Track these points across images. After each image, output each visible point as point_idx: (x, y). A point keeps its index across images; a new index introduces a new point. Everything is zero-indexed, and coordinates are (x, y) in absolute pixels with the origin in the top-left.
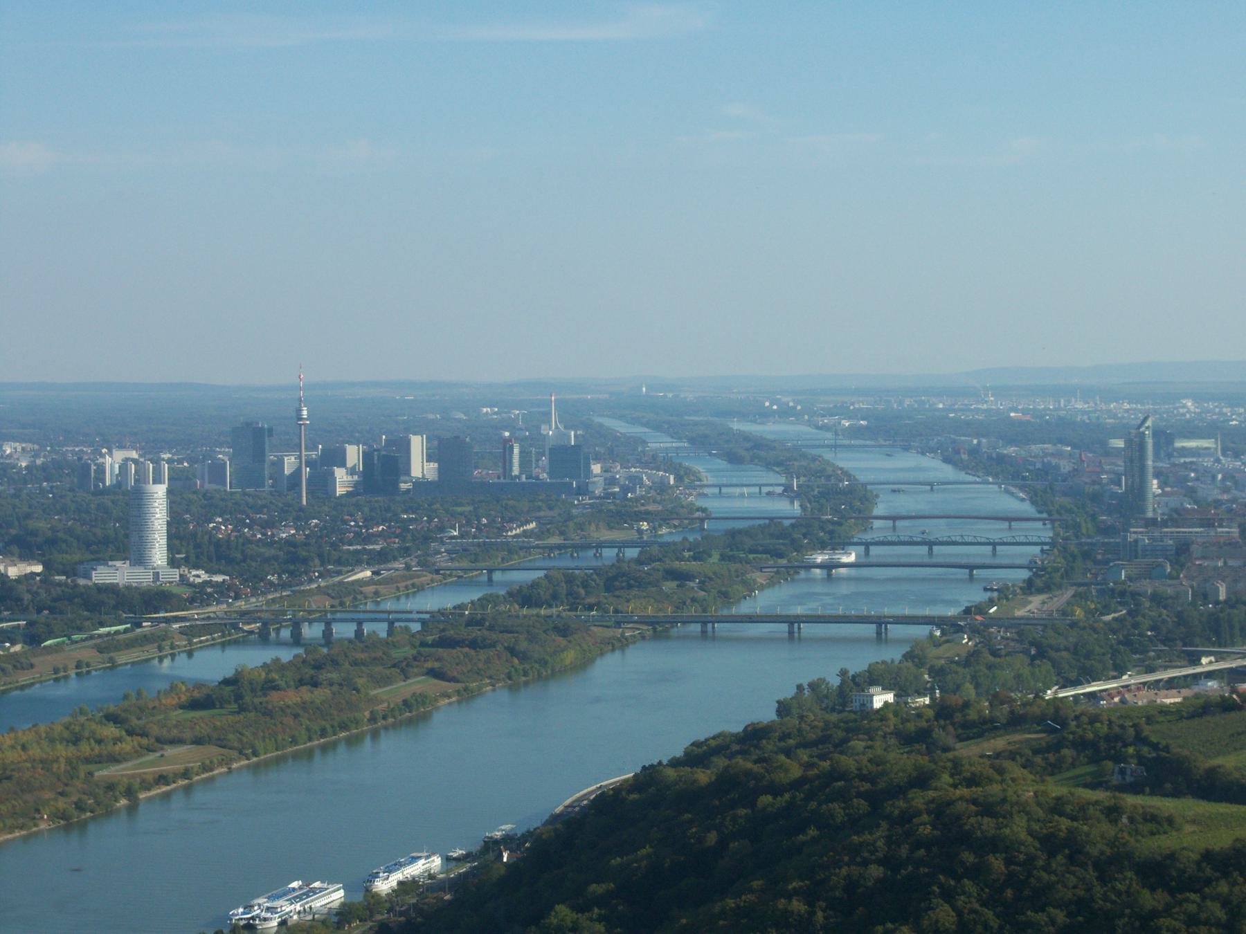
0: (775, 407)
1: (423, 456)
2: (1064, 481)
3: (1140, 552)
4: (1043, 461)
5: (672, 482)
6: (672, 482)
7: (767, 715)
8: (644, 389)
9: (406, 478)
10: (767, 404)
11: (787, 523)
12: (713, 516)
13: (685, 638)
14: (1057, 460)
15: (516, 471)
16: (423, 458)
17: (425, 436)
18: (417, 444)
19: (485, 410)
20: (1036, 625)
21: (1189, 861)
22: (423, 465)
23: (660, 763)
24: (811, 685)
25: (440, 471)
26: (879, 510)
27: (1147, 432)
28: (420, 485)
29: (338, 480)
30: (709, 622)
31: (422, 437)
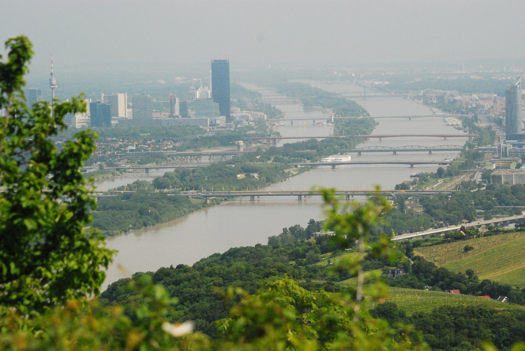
0: (340, 75)
1: (125, 105)
2: (486, 114)
3: (508, 154)
4: (476, 103)
5: (266, 118)
6: (266, 118)
7: (265, 242)
8: (270, 66)
9: (116, 118)
10: (335, 73)
11: (319, 140)
12: (282, 137)
13: (241, 204)
14: (483, 102)
15: (177, 112)
16: (125, 107)
17: (126, 94)
18: (122, 99)
19: (178, 78)
20: (430, 195)
21: (207, 308)
22: (125, 110)
23: (171, 267)
24: (290, 229)
25: (134, 113)
26: (375, 132)
27: (518, 86)
28: (123, 121)
29: (77, 119)
30: (302, 195)
31: (125, 94)
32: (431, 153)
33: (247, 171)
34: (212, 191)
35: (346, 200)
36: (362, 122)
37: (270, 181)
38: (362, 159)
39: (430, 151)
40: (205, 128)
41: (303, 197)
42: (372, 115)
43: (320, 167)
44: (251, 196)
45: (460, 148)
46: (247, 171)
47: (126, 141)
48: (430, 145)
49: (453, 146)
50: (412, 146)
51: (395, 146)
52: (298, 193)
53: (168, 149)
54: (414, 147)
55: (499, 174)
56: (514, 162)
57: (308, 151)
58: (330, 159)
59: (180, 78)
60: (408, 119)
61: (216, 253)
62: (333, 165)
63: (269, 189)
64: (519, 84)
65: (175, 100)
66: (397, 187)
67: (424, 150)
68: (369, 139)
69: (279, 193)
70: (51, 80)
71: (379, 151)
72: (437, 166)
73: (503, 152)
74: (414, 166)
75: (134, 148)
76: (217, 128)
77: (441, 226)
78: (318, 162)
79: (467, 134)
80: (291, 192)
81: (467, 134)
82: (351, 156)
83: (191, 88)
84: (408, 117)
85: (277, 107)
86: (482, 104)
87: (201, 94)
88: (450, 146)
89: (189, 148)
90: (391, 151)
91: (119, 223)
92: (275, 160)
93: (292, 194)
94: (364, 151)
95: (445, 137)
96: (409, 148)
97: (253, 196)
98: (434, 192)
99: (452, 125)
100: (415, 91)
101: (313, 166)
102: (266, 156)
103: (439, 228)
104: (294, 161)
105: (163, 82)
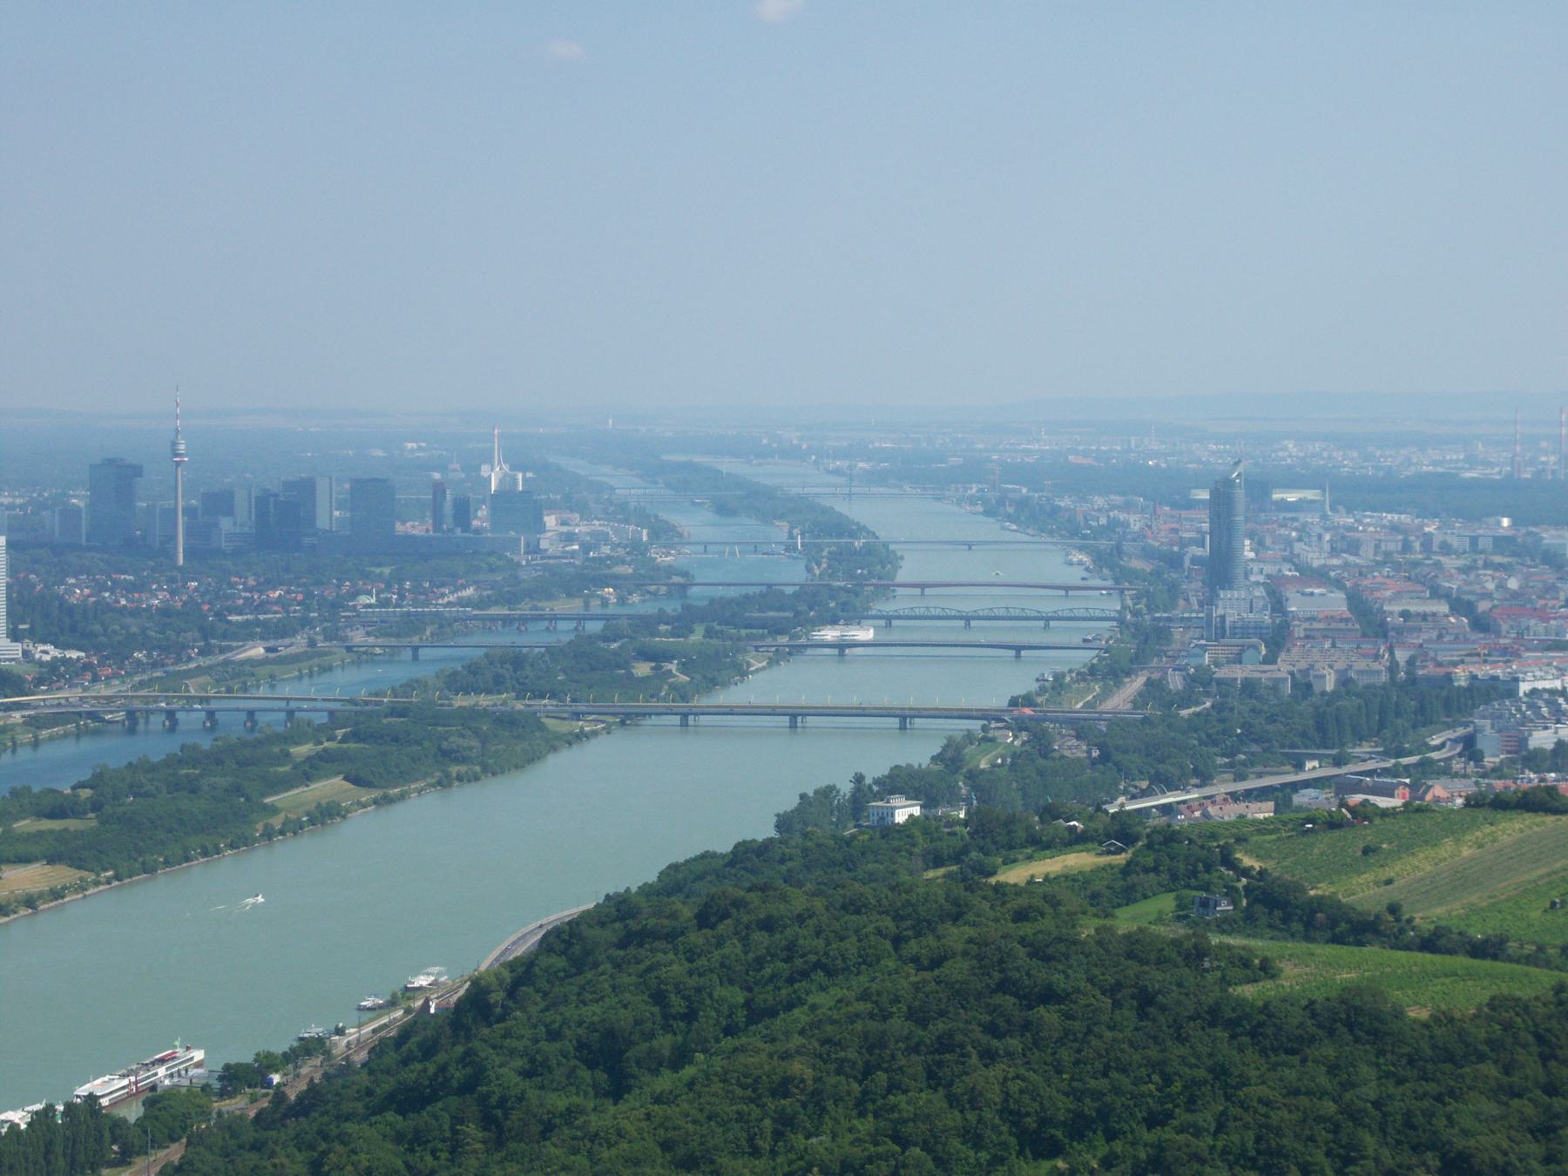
4: (1109, 517)
5: (645, 539)
19: (409, 445)
32: (891, 625)
33: (655, 656)
34: (588, 702)
35: (681, 726)
36: (869, 551)
37: (713, 683)
38: (894, 637)
39: (968, 619)
40: (516, 559)
41: (691, 718)
42: (883, 535)
43: (809, 651)
44: (681, 714)
45: (1113, 614)
46: (655, 656)
47: (347, 583)
48: (1047, 608)
49: (1017, 611)
50: (1007, 608)
51: (967, 607)
52: (790, 711)
53: (449, 604)
54: (1028, 612)
55: (1232, 675)
56: (1251, 649)
57: (772, 614)
58: (830, 634)
59: (415, 445)
60: (966, 547)
61: (708, 851)
62: (842, 646)
63: (723, 698)
64: (1238, 475)
65: (444, 492)
66: (1014, 702)
67: (1035, 618)
68: (894, 591)
69: (746, 710)
70: (174, 444)
71: (915, 618)
72: (484, 650)
73: (1216, 628)
74: (1023, 653)
75: (373, 601)
76: (541, 559)
77: (1145, 794)
78: (803, 641)
79: (1110, 583)
80: (774, 708)
81: (1110, 583)
82: (874, 627)
83: (451, 467)
84: (964, 543)
85: (665, 516)
86: (1122, 519)
87: (501, 482)
88: (1091, 611)
89: (496, 603)
90: (961, 618)
91: (401, 772)
92: (709, 633)
93: (773, 711)
94: (899, 617)
95: (923, 586)
96: (1002, 612)
97: (685, 716)
98: (1064, 712)
99: (1079, 564)
100: (959, 486)
101: (796, 650)
102: (682, 624)
103: (1141, 797)
104: (750, 637)
105: (380, 453)
